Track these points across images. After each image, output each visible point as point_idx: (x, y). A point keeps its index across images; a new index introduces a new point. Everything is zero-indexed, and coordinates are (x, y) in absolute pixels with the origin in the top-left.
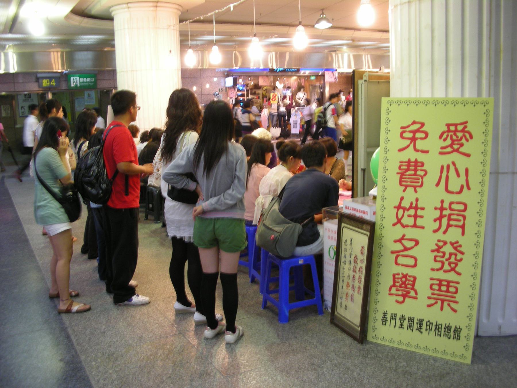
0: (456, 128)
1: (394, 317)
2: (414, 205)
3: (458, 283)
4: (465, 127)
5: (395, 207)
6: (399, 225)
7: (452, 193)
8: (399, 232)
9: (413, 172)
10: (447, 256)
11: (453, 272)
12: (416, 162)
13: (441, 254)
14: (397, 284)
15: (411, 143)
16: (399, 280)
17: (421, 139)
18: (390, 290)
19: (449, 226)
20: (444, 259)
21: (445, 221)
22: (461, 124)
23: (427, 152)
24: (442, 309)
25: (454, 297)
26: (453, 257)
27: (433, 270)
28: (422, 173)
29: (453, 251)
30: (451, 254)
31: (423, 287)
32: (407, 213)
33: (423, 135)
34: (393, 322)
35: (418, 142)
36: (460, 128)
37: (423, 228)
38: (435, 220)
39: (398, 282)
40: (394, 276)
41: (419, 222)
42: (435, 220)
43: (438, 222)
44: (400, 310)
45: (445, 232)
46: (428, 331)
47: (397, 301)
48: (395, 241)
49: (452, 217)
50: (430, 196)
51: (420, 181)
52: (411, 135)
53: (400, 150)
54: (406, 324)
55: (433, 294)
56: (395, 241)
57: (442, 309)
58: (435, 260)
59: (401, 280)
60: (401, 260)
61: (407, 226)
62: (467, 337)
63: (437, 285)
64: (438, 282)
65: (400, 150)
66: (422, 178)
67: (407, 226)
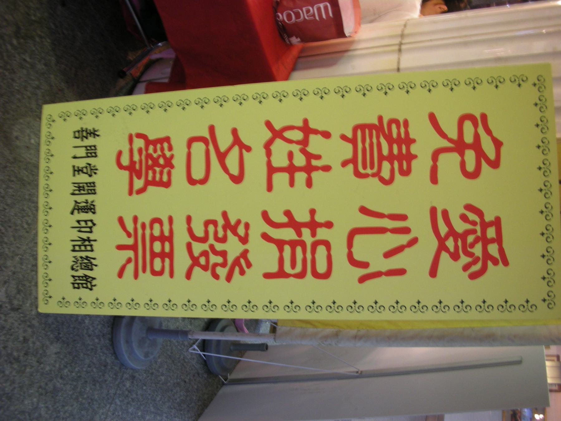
0: (492, 241)
1: (92, 152)
2: (314, 163)
3: (172, 275)
4: (495, 262)
5: (306, 121)
6: (268, 135)
7: (350, 244)
8: (255, 137)
9: (385, 152)
10: (219, 247)
11: (189, 262)
12: (411, 157)
13: (221, 234)
14: (151, 149)
15: (450, 140)
16: (159, 153)
17: (463, 164)
18: (139, 136)
19: (280, 244)
20: (211, 241)
21: (289, 234)
22: (501, 251)
23: (434, 179)
24: (120, 247)
25: (144, 271)
26: (219, 260)
27: (189, 219)
28: (386, 174)
29: (230, 259)
30: (223, 254)
31: (153, 204)
32: (296, 148)
33: (470, 167)
34: (82, 152)
35: (455, 157)
36: (493, 249)
37: (270, 188)
38: (288, 213)
39: (155, 151)
40: (167, 139)
41: (281, 179)
42: (288, 213)
43: (285, 220)
44: (105, 162)
45: (266, 237)
46: (77, 225)
47: (120, 154)
48: (235, 132)
49: (299, 250)
50: (338, 197)
51: (369, 171)
52: (469, 138)
53: (433, 118)
54: (83, 178)
55: (143, 226)
56: (235, 132)
57: (120, 247)
58: (207, 223)
59: (159, 157)
60: (198, 148)
61: (269, 153)
62: (80, 302)
63: (162, 231)
64: (167, 233)
65: (433, 118)
66: (374, 175)
67: (269, 153)
